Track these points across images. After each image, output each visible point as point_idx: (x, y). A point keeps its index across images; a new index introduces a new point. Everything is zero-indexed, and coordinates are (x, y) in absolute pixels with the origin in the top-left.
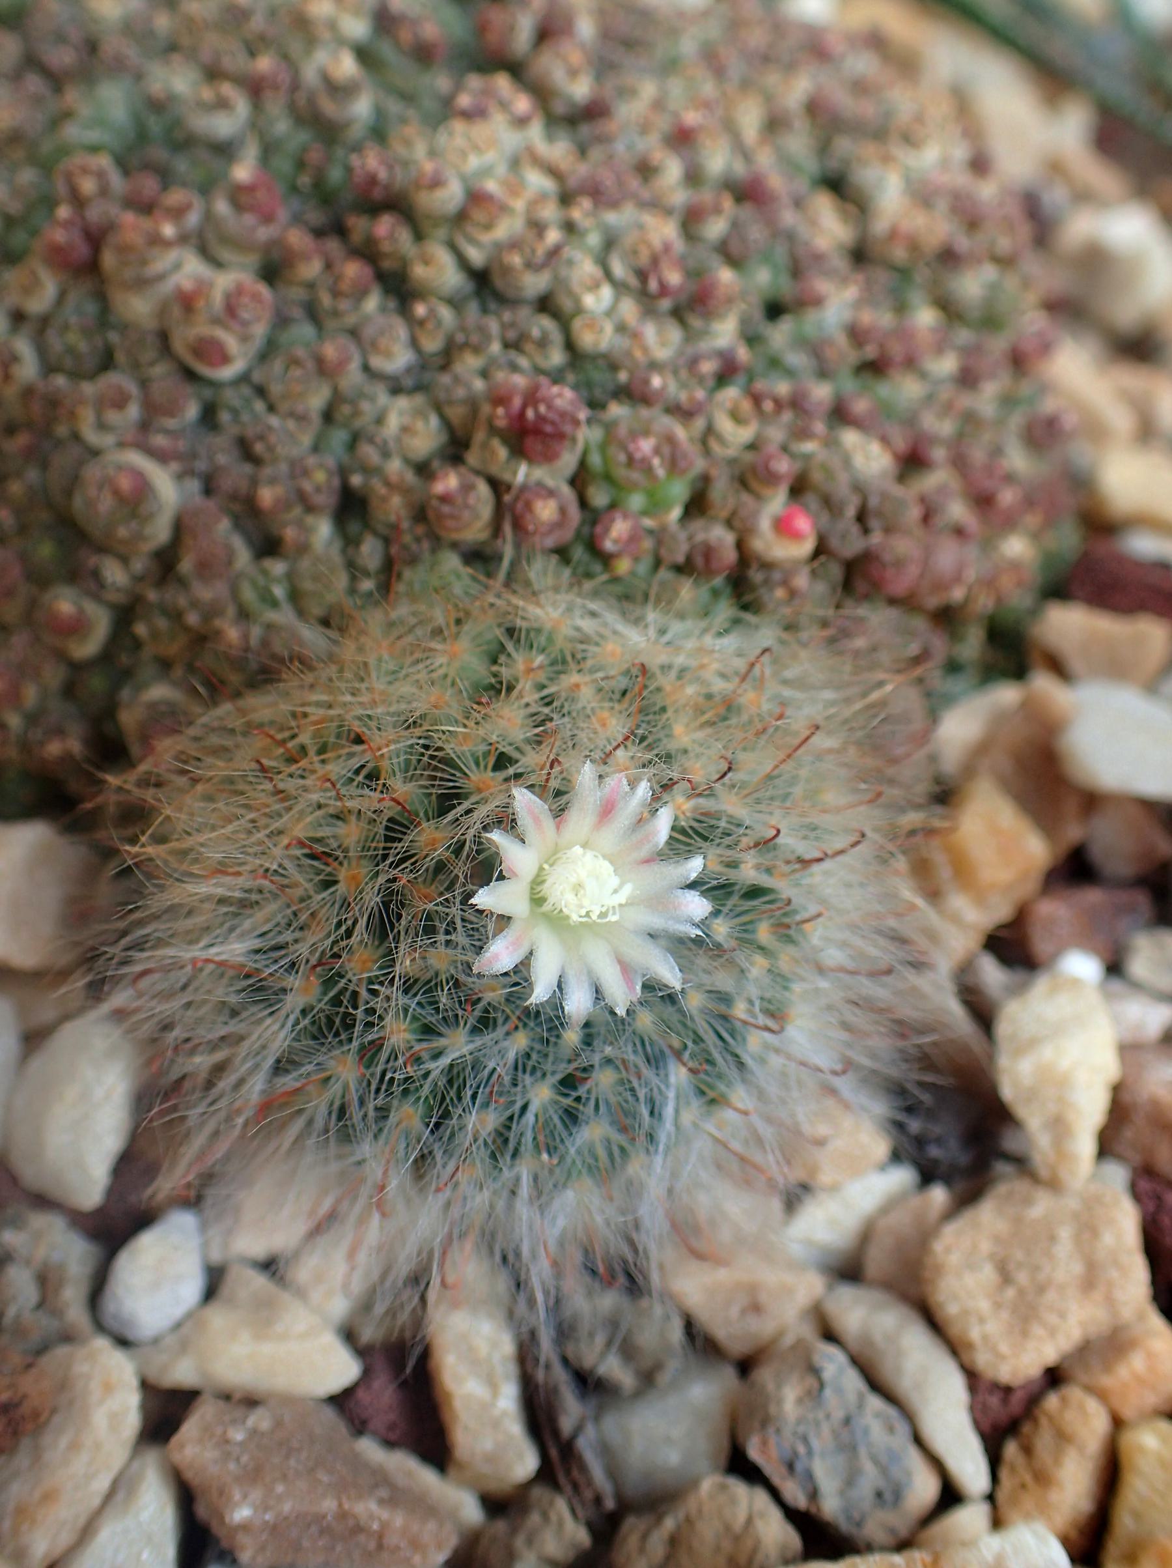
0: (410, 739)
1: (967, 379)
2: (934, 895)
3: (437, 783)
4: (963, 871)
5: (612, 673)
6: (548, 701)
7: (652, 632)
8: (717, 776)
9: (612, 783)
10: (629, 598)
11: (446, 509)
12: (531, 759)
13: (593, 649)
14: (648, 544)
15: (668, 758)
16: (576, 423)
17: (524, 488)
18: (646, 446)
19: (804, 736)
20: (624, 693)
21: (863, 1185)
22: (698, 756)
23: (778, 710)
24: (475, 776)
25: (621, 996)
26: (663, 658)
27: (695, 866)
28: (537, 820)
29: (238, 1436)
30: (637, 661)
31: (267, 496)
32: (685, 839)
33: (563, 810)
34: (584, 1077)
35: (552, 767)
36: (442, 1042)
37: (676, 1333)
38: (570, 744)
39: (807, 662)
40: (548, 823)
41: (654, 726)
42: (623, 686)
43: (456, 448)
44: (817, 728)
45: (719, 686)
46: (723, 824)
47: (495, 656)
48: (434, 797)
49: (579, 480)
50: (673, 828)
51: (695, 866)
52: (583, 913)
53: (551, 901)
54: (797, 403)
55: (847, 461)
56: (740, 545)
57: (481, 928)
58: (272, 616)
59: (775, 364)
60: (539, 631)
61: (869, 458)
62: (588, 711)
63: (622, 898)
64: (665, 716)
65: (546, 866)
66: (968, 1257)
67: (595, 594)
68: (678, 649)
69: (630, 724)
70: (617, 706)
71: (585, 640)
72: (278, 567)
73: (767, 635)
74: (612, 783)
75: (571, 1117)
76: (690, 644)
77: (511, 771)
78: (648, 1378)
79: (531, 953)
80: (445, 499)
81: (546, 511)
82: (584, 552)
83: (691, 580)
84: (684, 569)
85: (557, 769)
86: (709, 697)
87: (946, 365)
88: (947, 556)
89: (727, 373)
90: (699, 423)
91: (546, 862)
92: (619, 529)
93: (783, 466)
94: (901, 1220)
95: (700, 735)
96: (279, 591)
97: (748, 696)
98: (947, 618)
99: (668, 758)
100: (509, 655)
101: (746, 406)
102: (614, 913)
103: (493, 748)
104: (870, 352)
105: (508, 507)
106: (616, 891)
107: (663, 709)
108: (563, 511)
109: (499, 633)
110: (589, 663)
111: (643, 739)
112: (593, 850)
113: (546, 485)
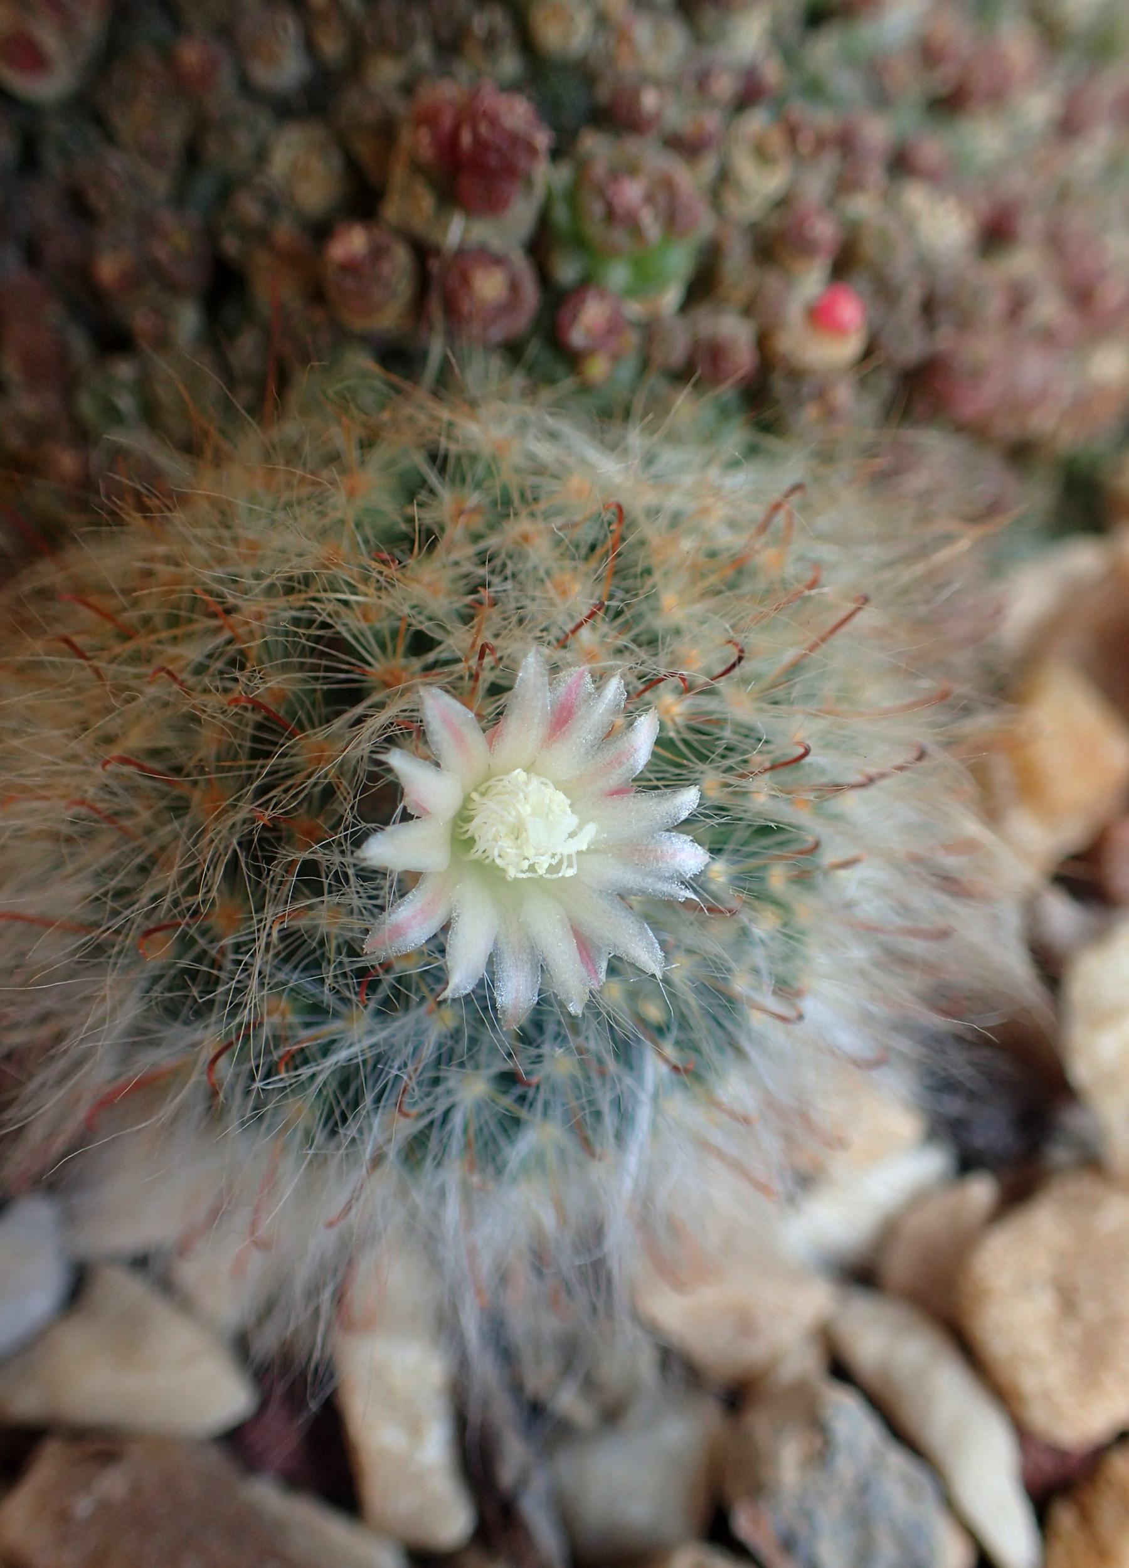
0: (284, 609)
1: (1068, 126)
2: (992, 815)
3: (321, 674)
4: (1030, 787)
5: (577, 518)
6: (483, 558)
7: (636, 462)
8: (722, 668)
9: (569, 680)
10: (609, 416)
11: (350, 283)
12: (456, 641)
13: (554, 485)
14: (632, 339)
15: (652, 642)
16: (532, 151)
17: (460, 252)
18: (632, 192)
19: (842, 614)
20: (593, 548)
21: (886, 1165)
22: (695, 640)
23: (809, 575)
24: (379, 667)
25: (574, 984)
26: (649, 498)
27: (688, 800)
28: (457, 735)
29: (83, 1506)
30: (612, 500)
31: (109, 268)
32: (674, 761)
33: (500, 713)
34: (527, 1069)
35: (482, 656)
36: (333, 1027)
37: (646, 1365)
38: (514, 619)
39: (846, 507)
40: (474, 737)
41: (636, 595)
42: (590, 539)
43: (362, 199)
44: (866, 600)
45: (726, 539)
46: (727, 733)
47: (413, 489)
48: (319, 695)
49: (541, 245)
50: (659, 742)
51: (688, 800)
52: (525, 865)
53: (480, 846)
54: (845, 142)
55: (910, 228)
56: (763, 341)
57: (382, 888)
58: (118, 437)
59: (814, 89)
60: (474, 458)
61: (941, 226)
62: (542, 573)
63: (582, 842)
64: (649, 582)
65: (475, 796)
66: (1018, 1277)
67: (558, 407)
68: (670, 488)
69: (600, 591)
70: (582, 567)
71: (540, 470)
72: (124, 370)
73: (793, 466)
74: (569, 680)
75: (511, 1124)
76: (688, 480)
77: (431, 657)
78: (612, 1415)
79: (446, 928)
80: (350, 267)
81: (489, 286)
82: (545, 348)
83: (688, 389)
84: (681, 376)
85: (488, 660)
86: (712, 555)
87: (1037, 107)
88: (1033, 369)
89: (750, 94)
90: (708, 166)
91: (475, 790)
92: (592, 315)
93: (824, 230)
94: (930, 1221)
95: (699, 608)
96: (126, 403)
97: (765, 557)
98: (1020, 453)
99: (652, 642)
100: (432, 492)
101: (776, 142)
102: (570, 866)
103: (402, 625)
104: (943, 78)
105: (435, 280)
106: (572, 835)
107: (648, 572)
108: (514, 287)
109: (419, 460)
110: (542, 506)
111: (619, 613)
112: (538, 774)
113: (489, 242)
